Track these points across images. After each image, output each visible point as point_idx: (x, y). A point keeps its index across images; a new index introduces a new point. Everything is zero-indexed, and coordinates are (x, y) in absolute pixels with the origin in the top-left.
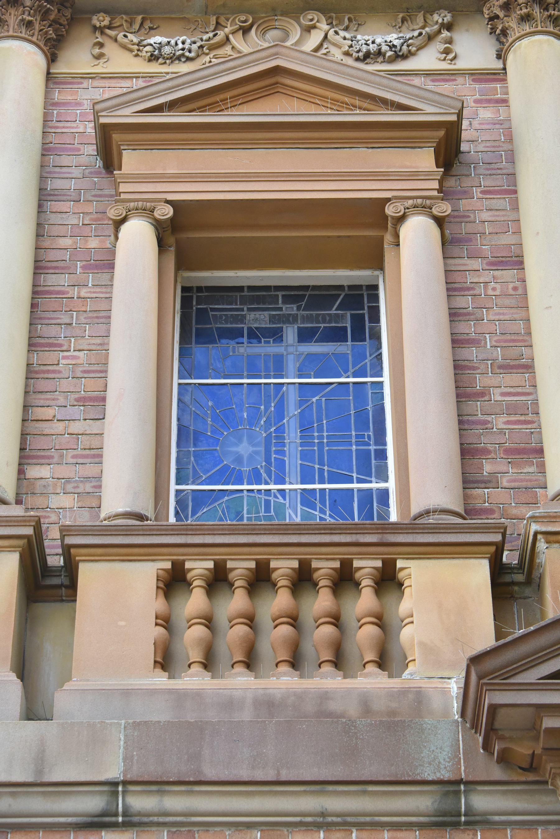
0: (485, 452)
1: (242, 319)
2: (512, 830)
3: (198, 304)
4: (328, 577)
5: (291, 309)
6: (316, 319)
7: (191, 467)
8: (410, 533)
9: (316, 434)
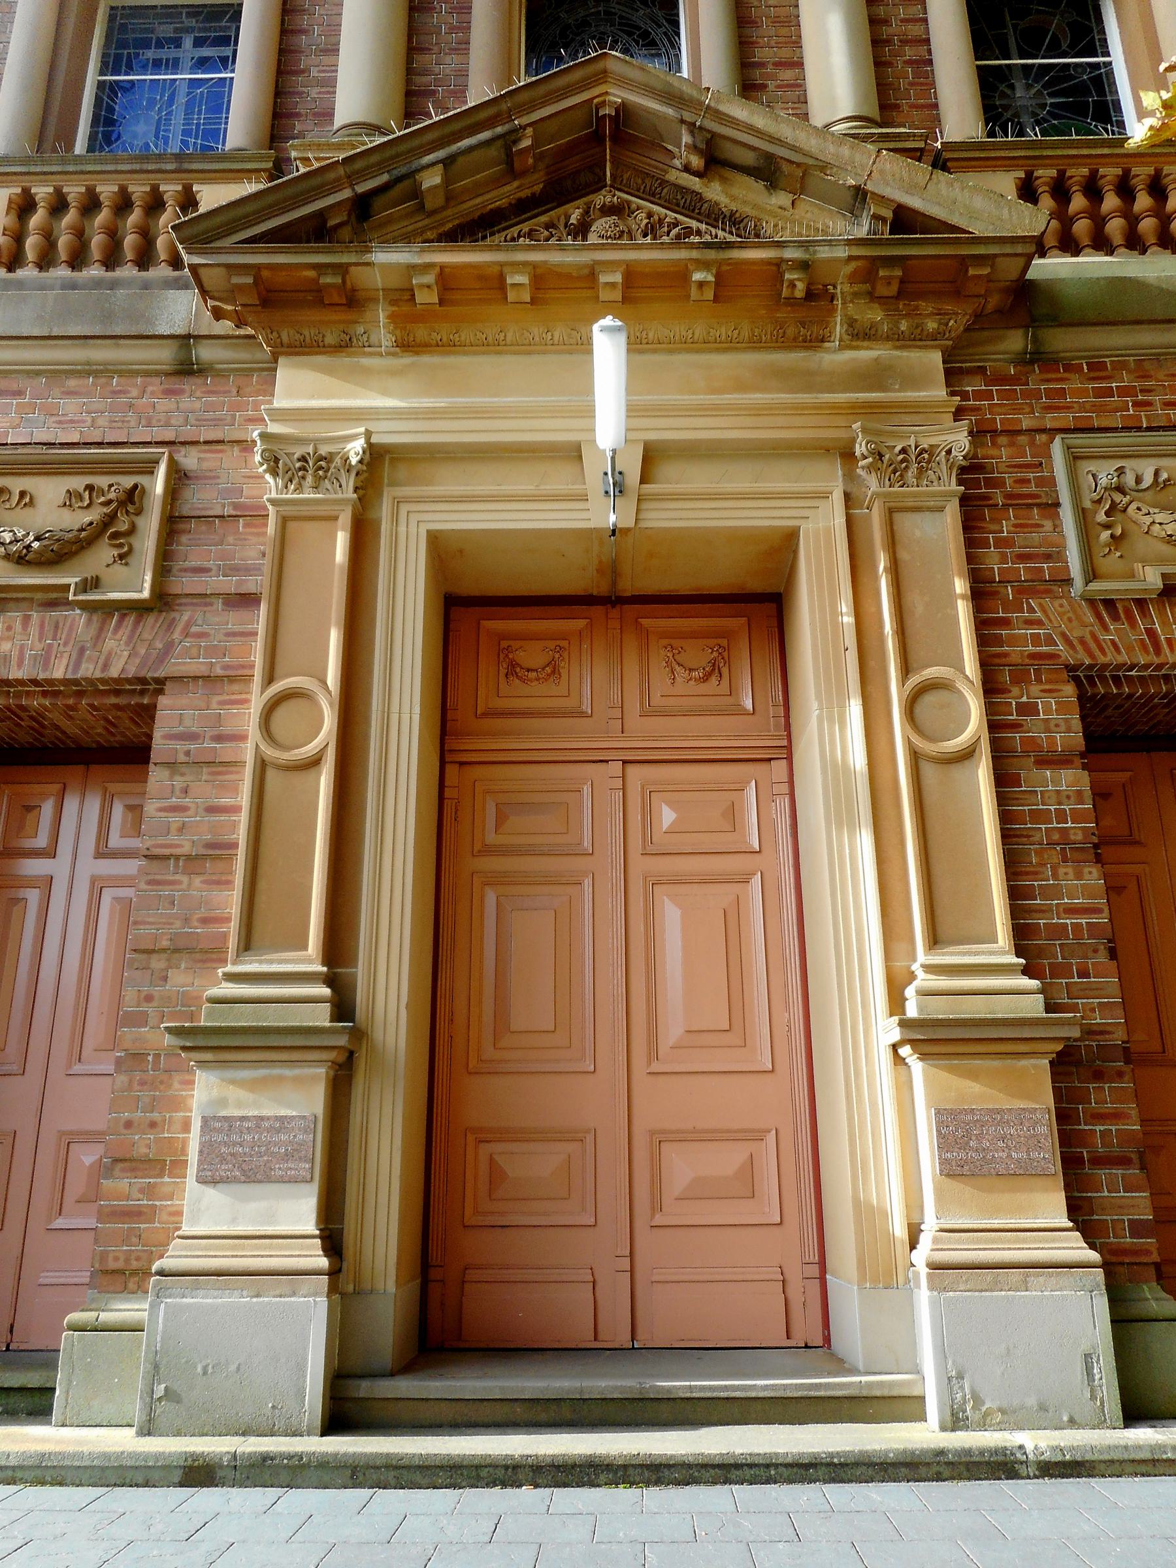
0: (298, 115)
3: (121, 19)
5: (192, 22)
6: (209, 30)
7: (98, 142)
9: (196, 116)
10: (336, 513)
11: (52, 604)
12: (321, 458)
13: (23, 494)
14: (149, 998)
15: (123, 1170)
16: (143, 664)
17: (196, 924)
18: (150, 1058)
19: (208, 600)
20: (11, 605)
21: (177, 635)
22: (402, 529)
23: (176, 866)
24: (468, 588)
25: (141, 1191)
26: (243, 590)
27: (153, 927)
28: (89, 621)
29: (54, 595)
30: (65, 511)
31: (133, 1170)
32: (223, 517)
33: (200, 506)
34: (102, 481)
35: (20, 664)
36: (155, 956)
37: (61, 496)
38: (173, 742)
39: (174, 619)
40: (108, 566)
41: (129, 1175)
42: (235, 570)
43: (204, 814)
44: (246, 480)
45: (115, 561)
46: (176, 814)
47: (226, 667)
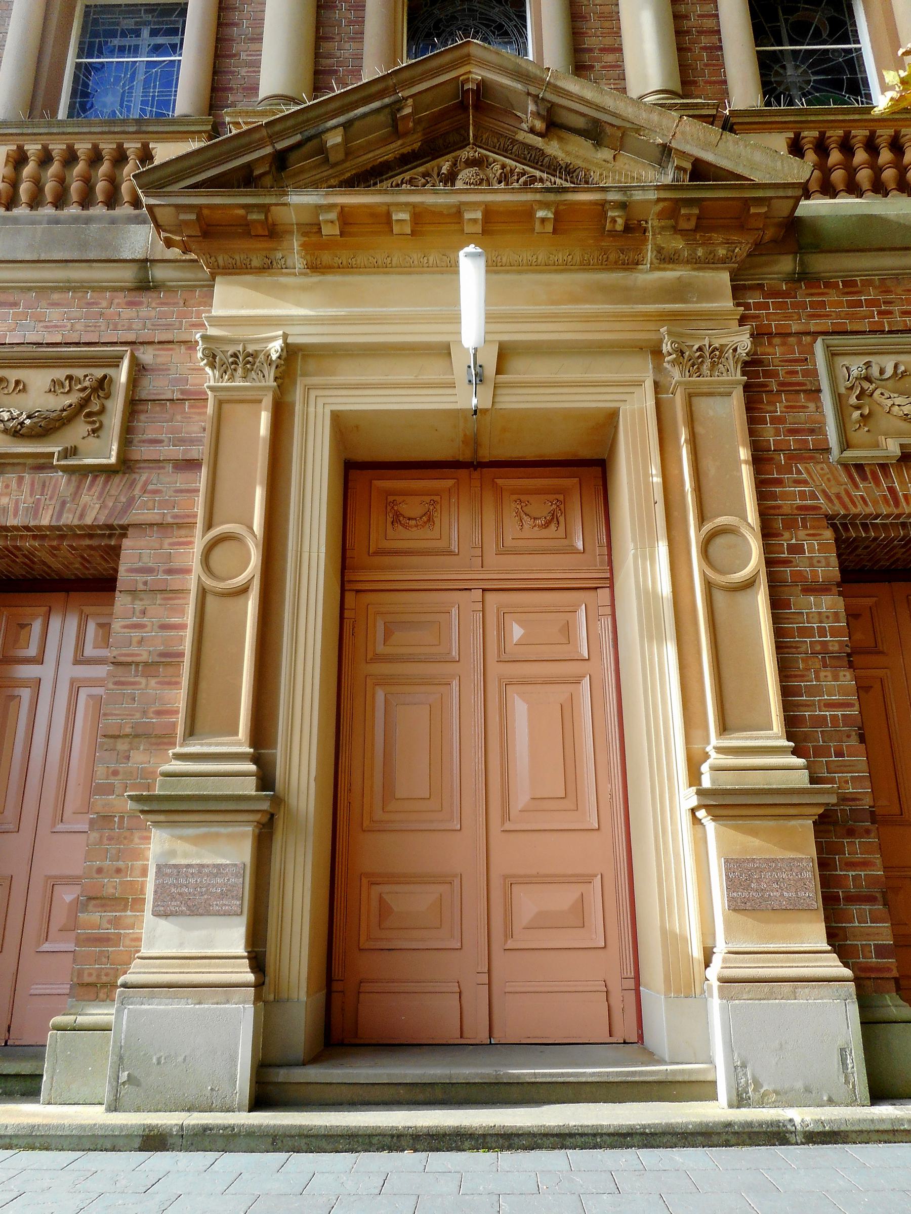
0: (231, 89)
1: (118, 24)
2: (181, 291)
3: (94, 15)
4: (110, 154)
5: (149, 17)
6: (162, 23)
7: (76, 110)
8: (520, 322)
9: (152, 90)
10: (260, 397)
11: (40, 468)
12: (249, 355)
13: (17, 383)
14: (115, 773)
15: (95, 906)
16: (110, 515)
17: (152, 715)
18: (116, 819)
19: (161, 464)
20: (9, 468)
21: (137, 492)
22: (312, 409)
23: (137, 671)
24: (363, 455)
25: (109, 922)
26: (188, 457)
27: (119, 718)
28: (69, 480)
29: (42, 461)
30: (51, 396)
31: (103, 906)
32: (173, 400)
33: (155, 392)
34: (79, 373)
35: (15, 514)
36: (120, 741)
37: (48, 384)
38: (134, 575)
39: (135, 479)
40: (84, 438)
41: (100, 909)
42: (181, 441)
43: (158, 630)
44: (191, 372)
45: (89, 434)
46: (136, 630)
47: (175, 516)
